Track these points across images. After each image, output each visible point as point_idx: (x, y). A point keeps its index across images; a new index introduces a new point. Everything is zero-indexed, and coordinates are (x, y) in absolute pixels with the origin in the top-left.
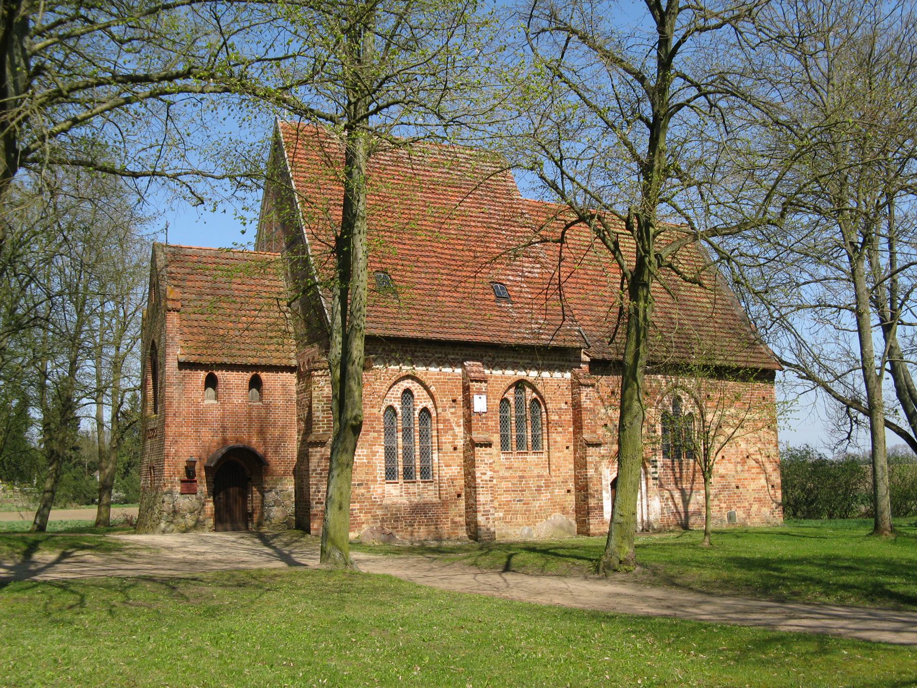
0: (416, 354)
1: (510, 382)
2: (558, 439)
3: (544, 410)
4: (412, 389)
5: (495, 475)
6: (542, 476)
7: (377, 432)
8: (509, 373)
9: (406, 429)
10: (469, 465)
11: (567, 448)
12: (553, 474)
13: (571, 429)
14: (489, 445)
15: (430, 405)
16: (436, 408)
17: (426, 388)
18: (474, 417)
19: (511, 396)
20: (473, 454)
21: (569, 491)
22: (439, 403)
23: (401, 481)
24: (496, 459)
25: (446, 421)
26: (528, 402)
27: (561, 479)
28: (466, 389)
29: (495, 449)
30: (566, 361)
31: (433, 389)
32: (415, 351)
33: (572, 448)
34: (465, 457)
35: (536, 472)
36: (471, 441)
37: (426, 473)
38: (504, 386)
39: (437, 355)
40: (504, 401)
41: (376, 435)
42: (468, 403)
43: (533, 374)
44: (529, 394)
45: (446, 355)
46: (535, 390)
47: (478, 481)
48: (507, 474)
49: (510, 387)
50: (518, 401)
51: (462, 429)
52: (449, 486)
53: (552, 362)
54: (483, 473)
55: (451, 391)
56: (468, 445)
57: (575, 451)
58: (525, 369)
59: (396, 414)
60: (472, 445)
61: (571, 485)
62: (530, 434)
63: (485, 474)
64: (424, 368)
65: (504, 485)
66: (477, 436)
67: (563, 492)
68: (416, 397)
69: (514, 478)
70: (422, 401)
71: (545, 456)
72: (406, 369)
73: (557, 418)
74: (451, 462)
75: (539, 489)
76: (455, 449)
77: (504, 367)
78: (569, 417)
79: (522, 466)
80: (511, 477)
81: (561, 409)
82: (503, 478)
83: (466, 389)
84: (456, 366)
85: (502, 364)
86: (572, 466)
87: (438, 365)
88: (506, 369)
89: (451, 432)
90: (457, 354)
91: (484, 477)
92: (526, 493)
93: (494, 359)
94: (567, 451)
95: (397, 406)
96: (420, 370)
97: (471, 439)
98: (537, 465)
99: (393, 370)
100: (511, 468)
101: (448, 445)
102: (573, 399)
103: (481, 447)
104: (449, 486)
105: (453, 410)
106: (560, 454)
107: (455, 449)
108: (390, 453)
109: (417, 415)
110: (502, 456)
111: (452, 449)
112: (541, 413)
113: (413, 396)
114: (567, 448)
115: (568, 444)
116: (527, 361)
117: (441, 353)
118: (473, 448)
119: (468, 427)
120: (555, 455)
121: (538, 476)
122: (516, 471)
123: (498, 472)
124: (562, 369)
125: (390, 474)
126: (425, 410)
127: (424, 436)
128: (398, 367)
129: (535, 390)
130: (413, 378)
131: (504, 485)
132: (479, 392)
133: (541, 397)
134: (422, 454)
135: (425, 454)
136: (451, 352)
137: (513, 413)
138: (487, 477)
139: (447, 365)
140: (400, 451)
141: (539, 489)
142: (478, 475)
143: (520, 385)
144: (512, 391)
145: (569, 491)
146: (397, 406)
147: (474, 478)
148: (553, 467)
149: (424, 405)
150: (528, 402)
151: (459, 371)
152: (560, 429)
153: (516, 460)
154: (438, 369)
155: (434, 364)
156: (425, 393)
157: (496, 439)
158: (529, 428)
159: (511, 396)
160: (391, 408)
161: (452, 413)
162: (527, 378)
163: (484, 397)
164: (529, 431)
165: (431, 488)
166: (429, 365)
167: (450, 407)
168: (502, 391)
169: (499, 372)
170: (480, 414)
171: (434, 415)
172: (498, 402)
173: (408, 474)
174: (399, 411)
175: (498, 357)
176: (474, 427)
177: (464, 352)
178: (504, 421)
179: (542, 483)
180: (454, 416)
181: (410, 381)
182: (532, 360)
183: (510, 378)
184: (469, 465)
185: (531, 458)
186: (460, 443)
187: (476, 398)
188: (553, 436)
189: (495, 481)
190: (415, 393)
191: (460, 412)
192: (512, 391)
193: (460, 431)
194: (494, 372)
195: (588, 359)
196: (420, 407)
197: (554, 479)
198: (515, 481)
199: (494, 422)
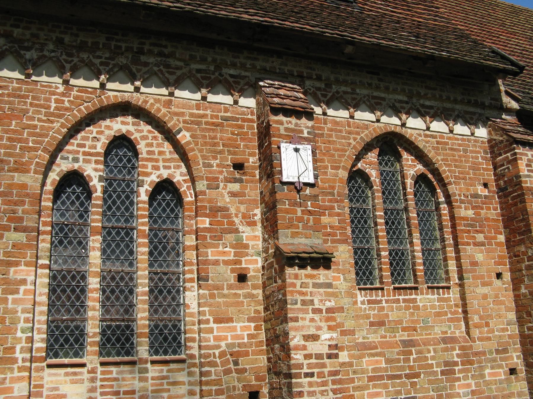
0: (143, 58)
1: (367, 135)
2: (480, 257)
3: (442, 199)
4: (135, 136)
5: (346, 340)
6: (453, 340)
7: (25, 230)
8: (364, 116)
9: (118, 230)
10: (276, 314)
11: (499, 276)
12: (476, 333)
13: (502, 238)
14: (323, 261)
15: (179, 176)
16: (193, 180)
17: (169, 135)
18: (283, 194)
19: (371, 165)
20: (282, 288)
21: (513, 371)
22: (199, 169)
23: (91, 357)
24: (345, 302)
25: (216, 211)
26: (409, 182)
27: (493, 345)
28: (265, 133)
29: (340, 278)
30: (476, 104)
31: (184, 137)
32: (141, 52)
33: (507, 276)
34: (267, 297)
35: (438, 331)
36: (278, 253)
37: (168, 340)
38: (355, 143)
39: (195, 66)
40: (357, 176)
41: (21, 237)
42: (269, 165)
43: (415, 123)
44: (412, 167)
45: (218, 68)
46: (420, 156)
47: (297, 357)
48: (374, 338)
49: (368, 148)
50: (391, 186)
51: (259, 231)
52: (227, 372)
53: (449, 105)
54: (310, 336)
55: (231, 145)
56: (271, 266)
57: (516, 283)
58: (397, 112)
59: (89, 193)
60: (283, 261)
61: (516, 359)
62: (418, 248)
63: (315, 338)
64: (164, 91)
65: (367, 363)
66: (291, 241)
67: (502, 374)
68: (143, 155)
69: (390, 345)
70: (157, 164)
71: (454, 295)
72: (119, 90)
73: (470, 213)
74: (231, 311)
75: (448, 371)
76: (242, 278)
77: (355, 104)
78: (493, 212)
79: (406, 317)
80: (383, 345)
81: (476, 196)
82: (366, 347)
83: (265, 133)
84: (242, 93)
85: (348, 97)
86: (512, 316)
87: (197, 86)
88: (357, 107)
89: (230, 238)
90: (243, 66)
91: (314, 348)
92: (422, 381)
93: (328, 85)
94: (498, 283)
95: (94, 173)
96: (152, 95)
97: (277, 248)
98: (438, 314)
99: (82, 89)
100: (381, 324)
101: (222, 268)
102: (498, 177)
103: (302, 267)
104: (227, 372)
105: (236, 187)
106: (485, 290)
107: (242, 278)
108: (66, 290)
109: (144, 197)
110: (360, 298)
111: (232, 278)
112: (438, 204)
113: (136, 154)
114: (499, 276)
115: (500, 269)
116: (400, 97)
117: (203, 60)
118: (282, 270)
119: (271, 225)
120: (477, 291)
121: (445, 340)
122: (393, 330)
123: (352, 332)
124: (470, 120)
125: (64, 341)
126: (165, 187)
127: (163, 249)
128: (95, 84)
129: (420, 156)
130: (140, 113)
131: (367, 363)
132: (294, 137)
133: (436, 172)
134: (155, 291)
135: (166, 292)
136: (229, 60)
137: (379, 201)
138: (320, 347)
139: (220, 87)
140: (94, 283)
141: (448, 371)
142: (296, 340)
143: (390, 145)
144: (373, 156)
145: (513, 371)
146: (94, 173)
147: (286, 349)
148: (475, 319)
149: (165, 174)
150: (409, 182)
151: (249, 102)
152: (480, 237)
153: (392, 305)
154: (198, 96)
155: (188, 83)
156: (167, 147)
157: (343, 254)
158: (416, 235)
159: (371, 165)
160: (74, 179)
161: (233, 194)
162: (403, 131)
163: (306, 150)
164: (417, 241)
165: (182, 377)
166: (178, 84)
167: (228, 180)
168: (351, 153)
169: (344, 114)
170: (297, 187)
171: (189, 198)
172: (344, 174)
173: (118, 342)
174: (97, 186)
175: (337, 82)
176: (282, 218)
177: (259, 64)
178: (360, 220)
179: (455, 355)
180: (239, 200)
181: (130, 119)
182: (410, 97)
183: (366, 127)
184: (276, 314)
185: (425, 299)
186: (254, 264)
187: (287, 150)
188: (468, 250)
189: (344, 356)
190: (142, 147)
191: (254, 192)
192: (373, 156)
193: (253, 235)
194: (330, 112)
195: (515, 105)
196: (154, 178)
197: (479, 346)
198: (394, 353)
199: (337, 217)
